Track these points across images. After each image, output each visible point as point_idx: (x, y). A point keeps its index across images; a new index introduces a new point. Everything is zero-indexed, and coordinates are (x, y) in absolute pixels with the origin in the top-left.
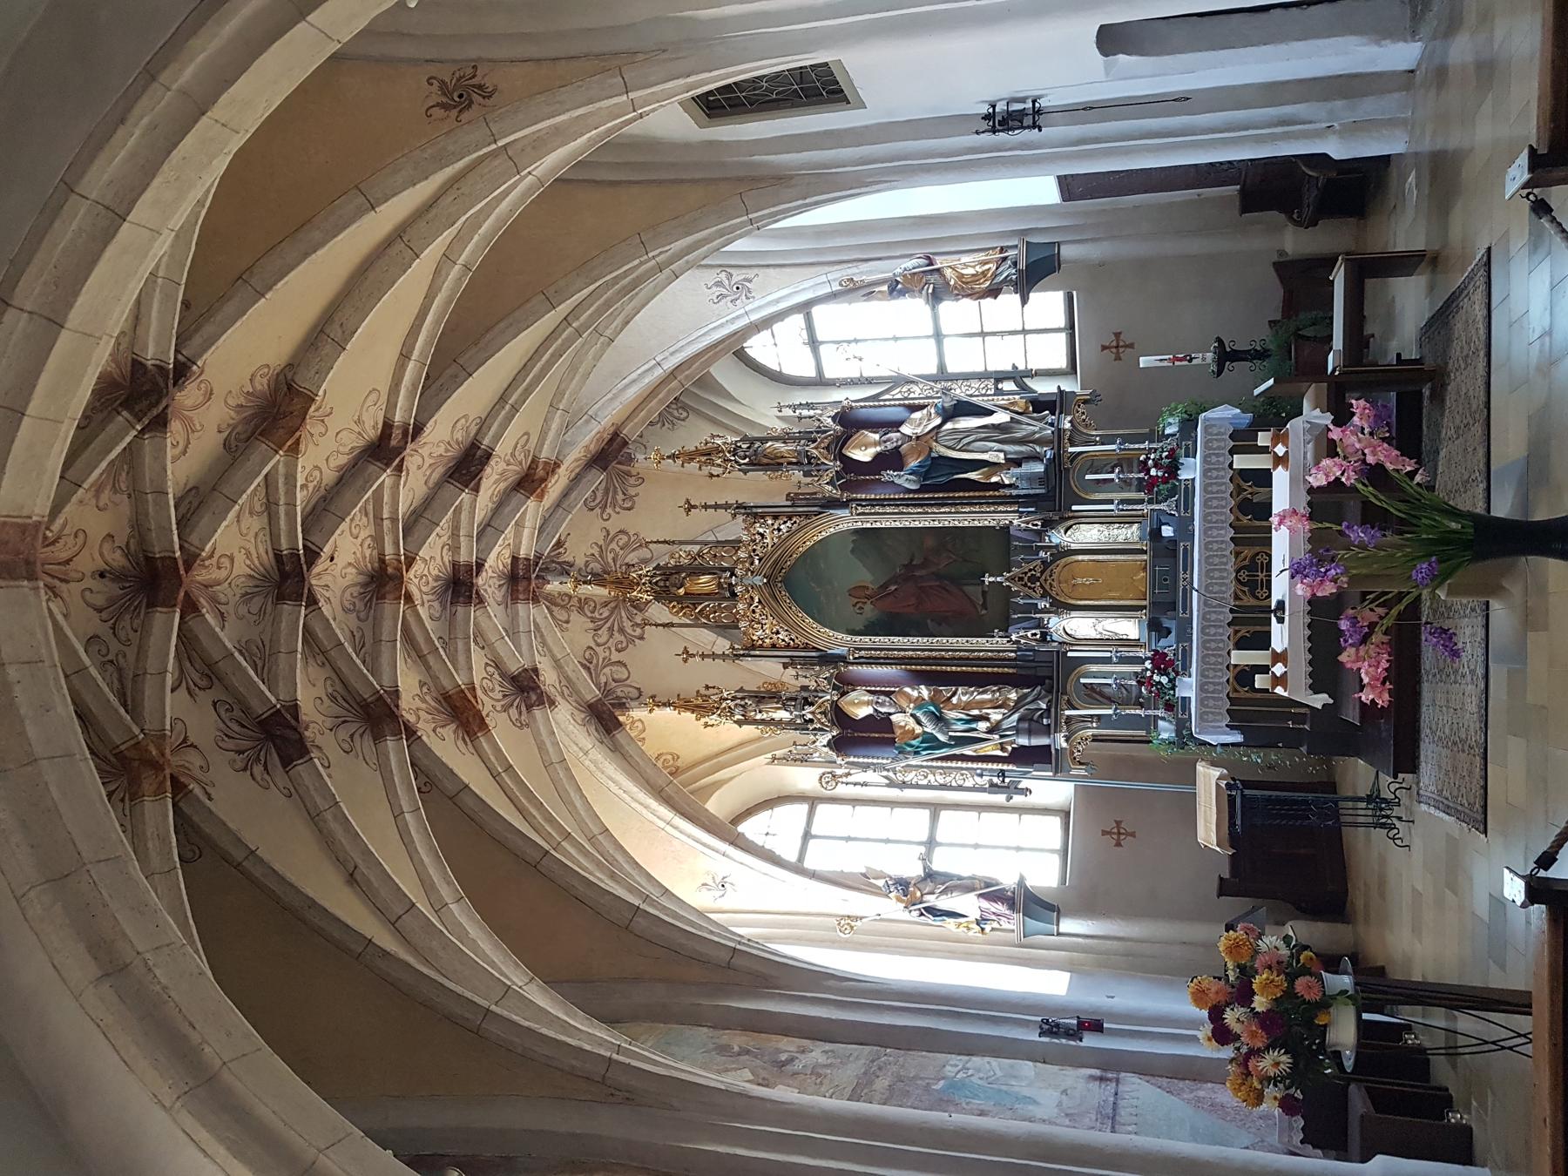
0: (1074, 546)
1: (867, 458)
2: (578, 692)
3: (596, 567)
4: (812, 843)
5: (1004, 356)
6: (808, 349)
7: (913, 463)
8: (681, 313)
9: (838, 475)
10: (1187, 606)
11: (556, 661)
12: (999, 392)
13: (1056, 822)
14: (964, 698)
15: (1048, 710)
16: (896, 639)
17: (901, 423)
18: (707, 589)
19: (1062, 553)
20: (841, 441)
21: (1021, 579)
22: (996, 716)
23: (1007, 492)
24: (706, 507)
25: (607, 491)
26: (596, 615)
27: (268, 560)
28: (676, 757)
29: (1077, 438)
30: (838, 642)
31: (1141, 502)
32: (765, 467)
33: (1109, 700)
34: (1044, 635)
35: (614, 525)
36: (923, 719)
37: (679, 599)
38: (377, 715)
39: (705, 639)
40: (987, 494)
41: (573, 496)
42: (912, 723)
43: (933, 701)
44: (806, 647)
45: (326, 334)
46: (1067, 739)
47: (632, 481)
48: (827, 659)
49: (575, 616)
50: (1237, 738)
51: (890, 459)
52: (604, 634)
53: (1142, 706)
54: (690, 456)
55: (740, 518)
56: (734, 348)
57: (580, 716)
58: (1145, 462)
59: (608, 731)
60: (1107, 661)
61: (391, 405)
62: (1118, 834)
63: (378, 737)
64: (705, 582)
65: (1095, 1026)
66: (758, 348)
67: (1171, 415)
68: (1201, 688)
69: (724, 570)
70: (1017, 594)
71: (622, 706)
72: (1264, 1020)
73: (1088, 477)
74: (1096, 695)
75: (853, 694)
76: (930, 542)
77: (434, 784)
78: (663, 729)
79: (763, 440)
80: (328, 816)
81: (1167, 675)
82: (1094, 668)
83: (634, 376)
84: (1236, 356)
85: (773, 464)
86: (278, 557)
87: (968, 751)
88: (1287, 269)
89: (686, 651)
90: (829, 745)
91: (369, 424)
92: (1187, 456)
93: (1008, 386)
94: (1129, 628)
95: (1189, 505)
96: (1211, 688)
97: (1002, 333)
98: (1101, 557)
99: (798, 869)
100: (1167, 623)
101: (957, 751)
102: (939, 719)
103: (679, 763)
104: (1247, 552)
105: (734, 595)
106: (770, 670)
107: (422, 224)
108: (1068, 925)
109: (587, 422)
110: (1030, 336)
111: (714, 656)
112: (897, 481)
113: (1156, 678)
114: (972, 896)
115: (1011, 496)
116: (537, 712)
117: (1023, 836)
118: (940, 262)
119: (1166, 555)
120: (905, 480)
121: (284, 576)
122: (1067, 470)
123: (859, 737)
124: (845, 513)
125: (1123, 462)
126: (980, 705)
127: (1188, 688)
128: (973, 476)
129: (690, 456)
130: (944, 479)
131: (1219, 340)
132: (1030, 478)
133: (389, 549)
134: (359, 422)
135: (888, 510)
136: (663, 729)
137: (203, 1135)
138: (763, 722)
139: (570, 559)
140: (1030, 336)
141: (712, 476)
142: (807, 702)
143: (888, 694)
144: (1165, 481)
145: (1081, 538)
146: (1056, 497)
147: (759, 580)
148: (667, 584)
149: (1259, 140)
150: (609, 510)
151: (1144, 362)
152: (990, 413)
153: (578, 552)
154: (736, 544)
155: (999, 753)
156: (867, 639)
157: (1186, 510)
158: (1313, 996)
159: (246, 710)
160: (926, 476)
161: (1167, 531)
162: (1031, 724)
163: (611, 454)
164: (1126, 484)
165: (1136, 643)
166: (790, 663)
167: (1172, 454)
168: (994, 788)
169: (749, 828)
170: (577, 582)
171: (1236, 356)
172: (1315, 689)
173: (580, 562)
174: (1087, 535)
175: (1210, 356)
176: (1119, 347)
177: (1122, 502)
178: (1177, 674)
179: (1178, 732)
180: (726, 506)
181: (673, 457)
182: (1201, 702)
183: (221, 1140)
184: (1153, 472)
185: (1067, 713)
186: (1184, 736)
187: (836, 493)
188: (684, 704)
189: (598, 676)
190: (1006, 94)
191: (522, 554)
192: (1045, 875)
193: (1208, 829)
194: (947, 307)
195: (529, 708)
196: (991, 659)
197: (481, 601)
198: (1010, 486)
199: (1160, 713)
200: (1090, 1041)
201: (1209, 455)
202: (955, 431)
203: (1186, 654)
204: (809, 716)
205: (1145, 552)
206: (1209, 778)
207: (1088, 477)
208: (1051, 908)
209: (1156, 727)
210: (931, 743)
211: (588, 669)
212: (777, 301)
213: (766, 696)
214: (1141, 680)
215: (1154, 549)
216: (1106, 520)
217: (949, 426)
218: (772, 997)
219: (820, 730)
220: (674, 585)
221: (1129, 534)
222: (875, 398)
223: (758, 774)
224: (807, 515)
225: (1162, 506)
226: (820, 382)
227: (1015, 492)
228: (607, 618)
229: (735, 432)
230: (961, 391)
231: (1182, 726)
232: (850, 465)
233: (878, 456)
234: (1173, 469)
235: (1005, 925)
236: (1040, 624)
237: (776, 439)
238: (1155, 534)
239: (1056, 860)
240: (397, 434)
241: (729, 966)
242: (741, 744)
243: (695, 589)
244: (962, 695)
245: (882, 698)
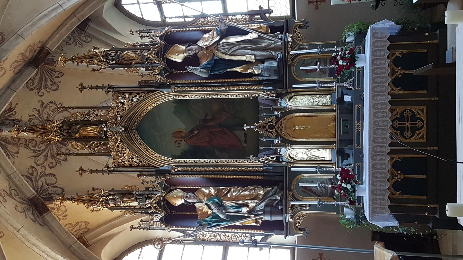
0: (294, 108)
1: (180, 60)
2: (22, 193)
7: (204, 62)
10: (360, 141)
11: (8, 176)
14: (234, 194)
15: (281, 200)
16: (198, 160)
19: (287, 112)
20: (162, 52)
21: (264, 127)
23: (257, 78)
25: (41, 80)
26: (37, 148)
28: (87, 223)
30: (166, 162)
31: (332, 82)
34: (278, 158)
35: (47, 98)
36: (212, 207)
40: (246, 79)
41: (17, 82)
42: (206, 209)
43: (217, 196)
44: (149, 166)
46: (292, 217)
47: (56, 74)
48: (160, 172)
49: (23, 150)
51: (192, 60)
52: (41, 158)
55: (111, 94)
57: (21, 207)
58: (335, 57)
59: (41, 214)
67: (350, 31)
69: (101, 123)
70: (262, 136)
71: (51, 199)
73: (302, 68)
74: (309, 192)
75: (175, 192)
76: (216, 107)
79: (123, 50)
81: (350, 183)
82: (307, 176)
83: (46, 12)
85: (127, 63)
89: (81, 169)
90: (161, 220)
92: (359, 53)
94: (325, 154)
95: (360, 82)
96: (378, 192)
98: (309, 114)
102: (220, 206)
103: (89, 226)
104: (398, 109)
105: (107, 137)
106: (131, 180)
109: (16, 38)
111: (97, 171)
112: (195, 72)
113: (344, 185)
115: (259, 81)
120: (200, 72)
122: (290, 65)
123: (175, 216)
124: (168, 91)
125: (323, 61)
126: (244, 198)
128: (238, 69)
129: (81, 59)
130: (222, 71)
132: (269, 70)
135: (192, 89)
138: (125, 208)
139: (19, 118)
141: (94, 70)
142: (149, 198)
144: (348, 68)
145: (298, 104)
146: (284, 80)
147: (121, 129)
150: (43, 90)
152: (246, 33)
153: (24, 113)
154: (108, 109)
155: (254, 224)
156: (182, 160)
157: (358, 86)
161: (347, 98)
162: (272, 208)
163: (40, 59)
165: (329, 162)
166: (141, 174)
167: (352, 52)
170: (19, 131)
174: (301, 101)
177: (321, 82)
178: (356, 183)
179: (357, 216)
180: (103, 87)
181: (72, 60)
184: (340, 63)
185: (292, 203)
187: (164, 80)
188: (80, 199)
189: (37, 182)
196: (250, 171)
198: (258, 75)
199: (345, 204)
201: (375, 51)
202: (227, 44)
203: (360, 170)
204: (149, 205)
205: (334, 111)
207: (302, 68)
209: (343, 211)
210: (217, 220)
211: (31, 179)
213: (125, 194)
215: (340, 109)
216: (312, 93)
217: (224, 41)
219: (155, 213)
220: (74, 132)
221: (325, 101)
225: (345, 84)
227: (261, 78)
228: (44, 150)
229: (107, 44)
231: (359, 212)
232: (171, 64)
234: (352, 61)
236: (275, 152)
237: (130, 50)
238: (340, 101)
243: (86, 134)
244: (234, 192)
245: (190, 194)
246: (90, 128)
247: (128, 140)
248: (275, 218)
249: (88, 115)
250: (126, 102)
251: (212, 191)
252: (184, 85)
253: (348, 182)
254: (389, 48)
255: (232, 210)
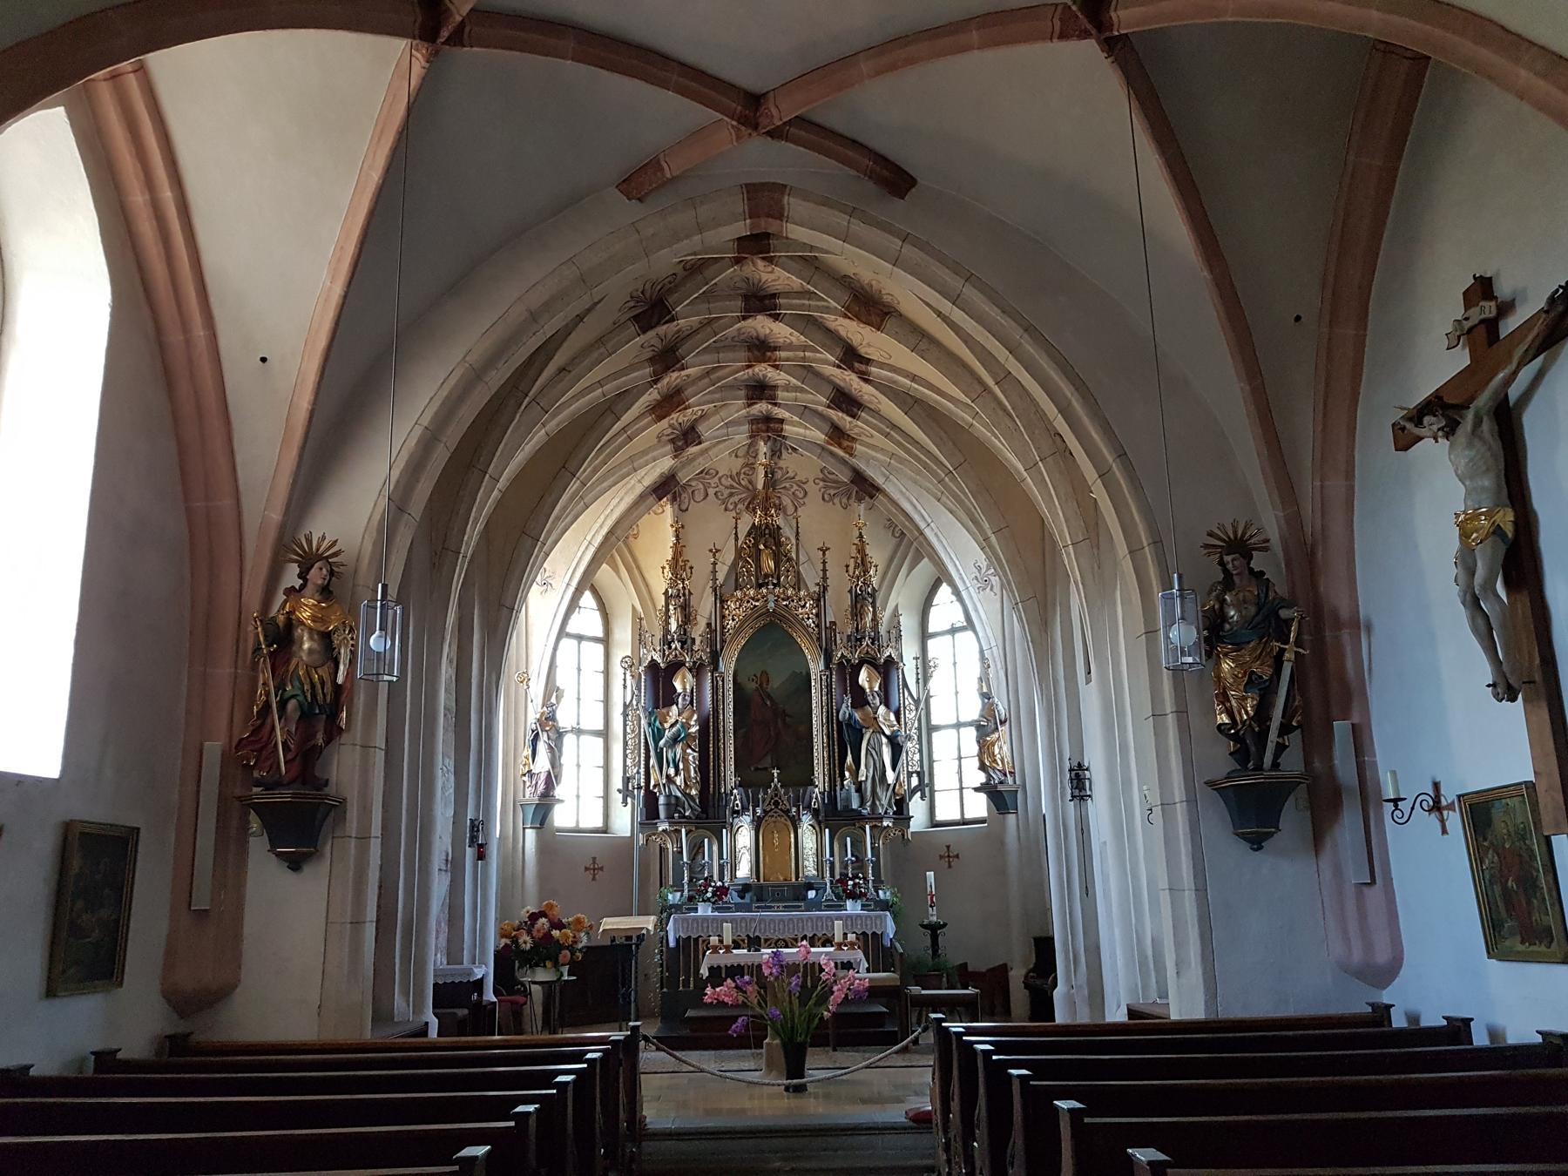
3: (779, 474)
4: (575, 642)
5: (944, 777)
6: (948, 627)
7: (857, 716)
8: (961, 548)
9: (848, 661)
12: (910, 775)
13: (599, 823)
17: (887, 706)
18: (764, 566)
19: (795, 823)
20: (872, 662)
22: (679, 780)
24: (824, 563)
27: (772, 290)
29: (876, 832)
30: (728, 665)
31: (832, 875)
32: (854, 606)
33: (693, 858)
34: (737, 812)
35: (810, 487)
37: (756, 545)
38: (667, 359)
39: (728, 556)
44: (723, 641)
45: (919, 339)
48: (715, 657)
50: (672, 944)
51: (860, 698)
53: (690, 880)
54: (861, 551)
56: (941, 577)
60: (721, 857)
61: (882, 365)
62: (594, 869)
63: (652, 360)
64: (769, 564)
65: (481, 855)
66: (944, 591)
68: (705, 919)
71: (674, 499)
72: (548, 935)
74: (696, 850)
76: (802, 728)
77: (624, 398)
78: (658, 535)
79: (874, 604)
80: (602, 350)
82: (715, 848)
84: (935, 938)
85: (857, 612)
86: (774, 296)
87: (653, 761)
88: (1000, 973)
91: (870, 350)
93: (915, 781)
94: (744, 870)
97: (960, 772)
99: (562, 633)
100: (748, 896)
101: (652, 753)
102: (675, 740)
105: (760, 586)
106: (705, 607)
107: (993, 405)
108: (531, 835)
110: (955, 794)
114: (548, 766)
116: (669, 447)
117: (590, 796)
118: (1003, 729)
119: (797, 893)
120: (845, 710)
121: (762, 299)
123: (659, 682)
124: (822, 667)
126: (686, 769)
127: (704, 910)
128: (849, 759)
130: (847, 738)
131: (945, 925)
132: (848, 799)
133: (783, 354)
134: (869, 345)
136: (658, 535)
137: (452, 381)
138: (668, 610)
140: (955, 794)
142: (683, 643)
143: (691, 702)
144: (845, 891)
146: (834, 817)
148: (766, 535)
149: (1065, 944)
151: (930, 874)
153: (788, 462)
158: (561, 958)
159: (670, 291)
160: (849, 725)
161: (811, 894)
163: (863, 487)
164: (844, 865)
167: (862, 895)
168: (626, 780)
169: (588, 599)
170: (766, 466)
171: (935, 938)
172: (711, 969)
173: (782, 463)
175: (934, 919)
176: (949, 857)
177: (832, 864)
179: (672, 906)
180: (825, 578)
182: (695, 919)
183: (450, 393)
186: (666, 910)
187: (836, 660)
190: (1094, 779)
191: (786, 427)
192: (562, 818)
193: (609, 923)
194: (970, 734)
195: (672, 441)
197: (749, 405)
200: (470, 852)
202: (881, 745)
206: (649, 923)
208: (542, 823)
212: (976, 610)
214: (709, 880)
215: (800, 886)
216: (819, 852)
217: (884, 740)
218: (483, 637)
221: (810, 868)
222: (905, 685)
223: (626, 602)
224: (819, 639)
226: (924, 636)
230: (910, 746)
233: (863, 689)
234: (853, 896)
235: (528, 792)
236: (745, 809)
239: (571, 824)
240: (863, 367)
241: (501, 605)
242: (652, 599)
243: (764, 557)
244: (692, 755)
246: (772, 564)
247: (756, 614)
248: (662, 809)
249: (790, 560)
250: (806, 611)
251: (693, 730)
252: (829, 686)
253: (714, 894)
254: (864, 933)
255: (670, 756)
